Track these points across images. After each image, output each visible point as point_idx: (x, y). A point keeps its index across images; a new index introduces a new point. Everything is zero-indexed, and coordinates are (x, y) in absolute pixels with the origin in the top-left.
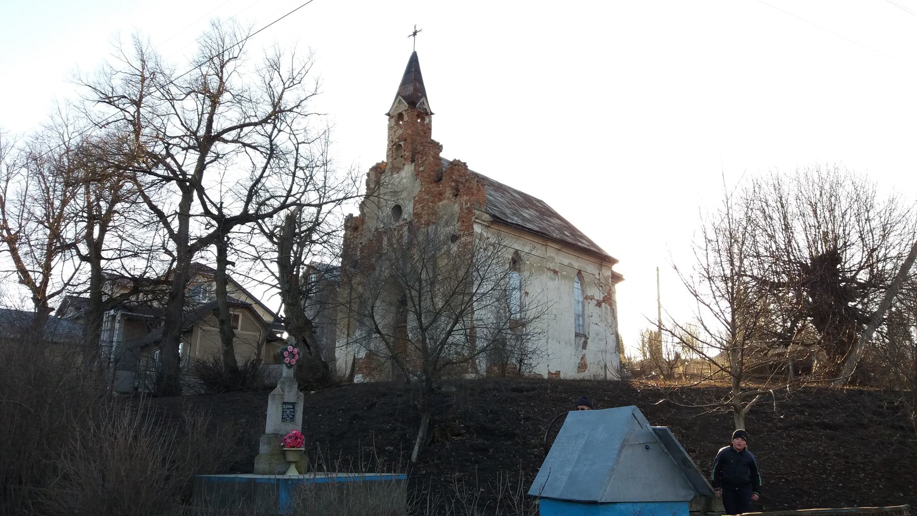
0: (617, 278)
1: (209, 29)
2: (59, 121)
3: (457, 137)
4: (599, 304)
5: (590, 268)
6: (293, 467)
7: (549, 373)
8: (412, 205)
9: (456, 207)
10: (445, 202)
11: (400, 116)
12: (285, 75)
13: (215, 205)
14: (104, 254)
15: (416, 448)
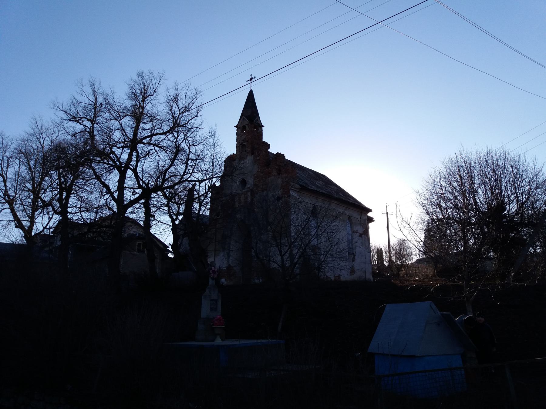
0: (371, 220)
1: (135, 77)
2: (37, 130)
3: (278, 139)
4: (361, 235)
5: (355, 215)
6: (218, 337)
7: (334, 276)
8: (253, 179)
9: (280, 181)
10: (272, 177)
11: (244, 128)
12: (181, 105)
13: (145, 183)
14: (69, 210)
15: (281, 324)
